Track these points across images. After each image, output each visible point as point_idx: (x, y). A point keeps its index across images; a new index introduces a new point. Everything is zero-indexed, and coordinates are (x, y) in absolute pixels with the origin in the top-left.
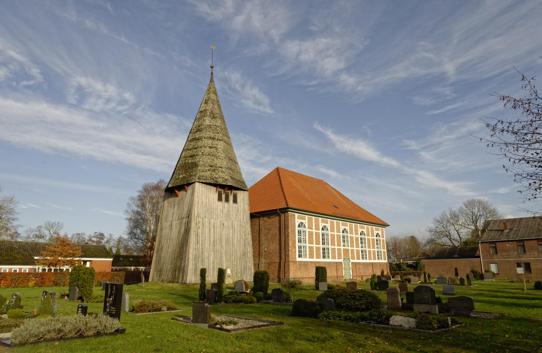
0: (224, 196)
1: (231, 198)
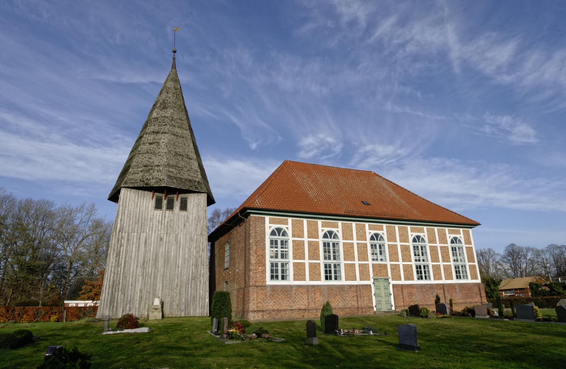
0: (165, 202)
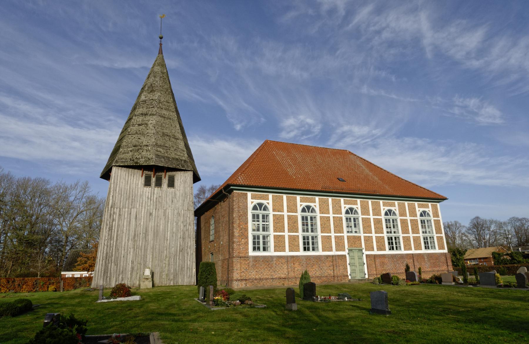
0: (153, 180)
1: (165, 182)
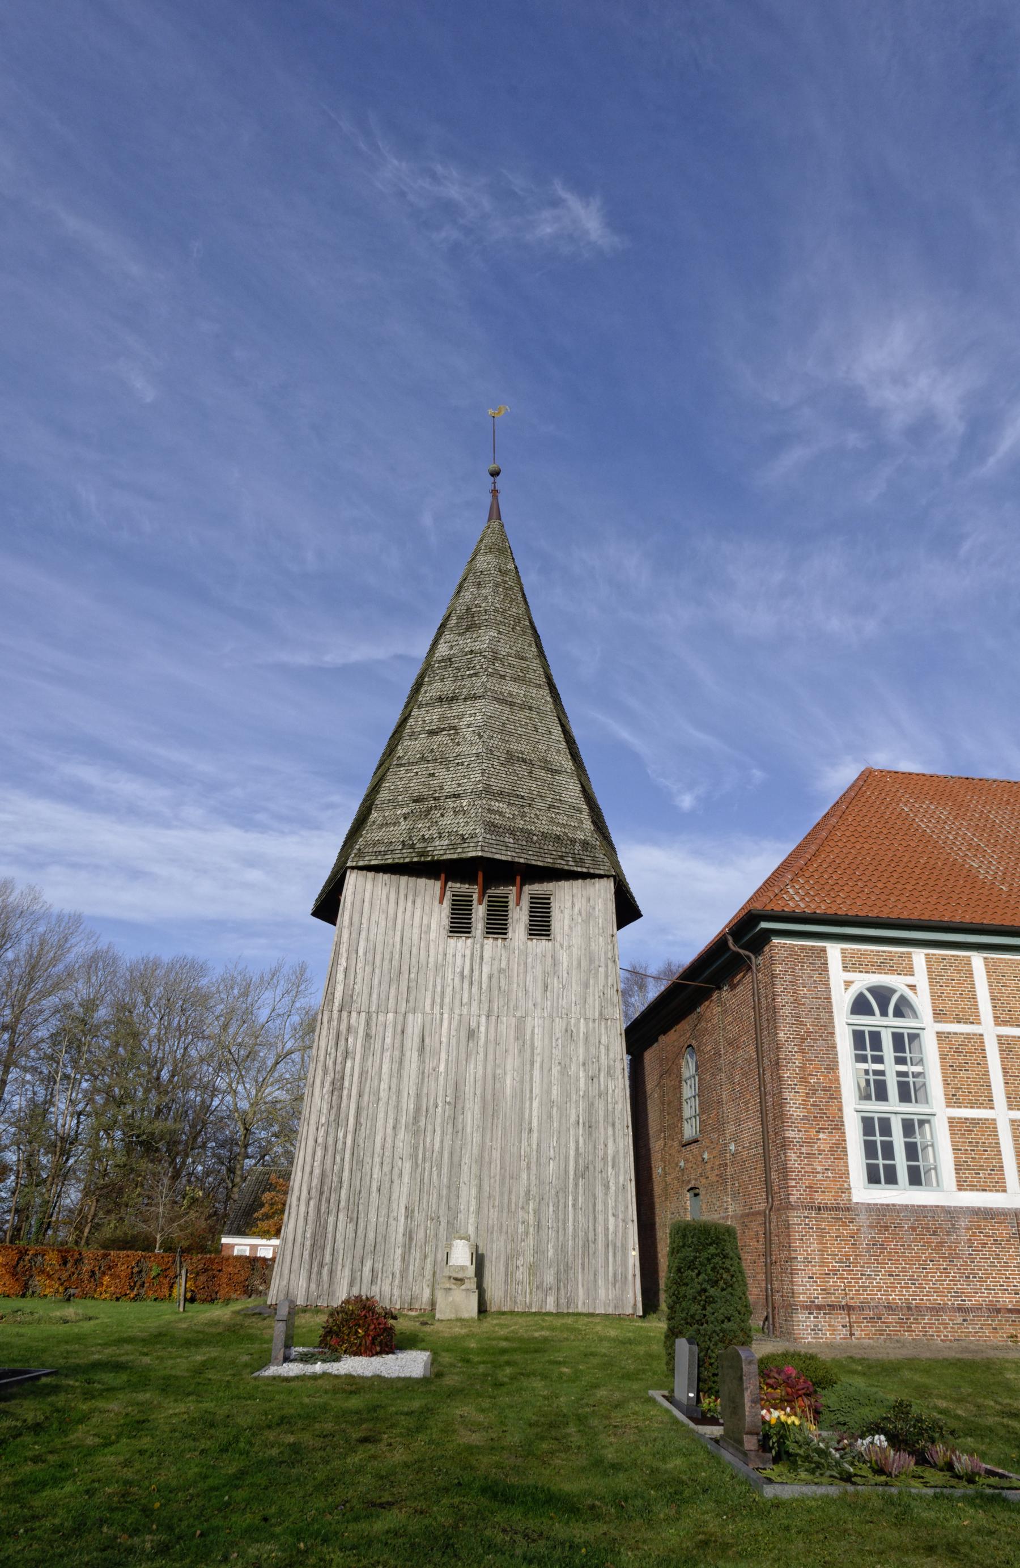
0: (479, 912)
1: (519, 917)
